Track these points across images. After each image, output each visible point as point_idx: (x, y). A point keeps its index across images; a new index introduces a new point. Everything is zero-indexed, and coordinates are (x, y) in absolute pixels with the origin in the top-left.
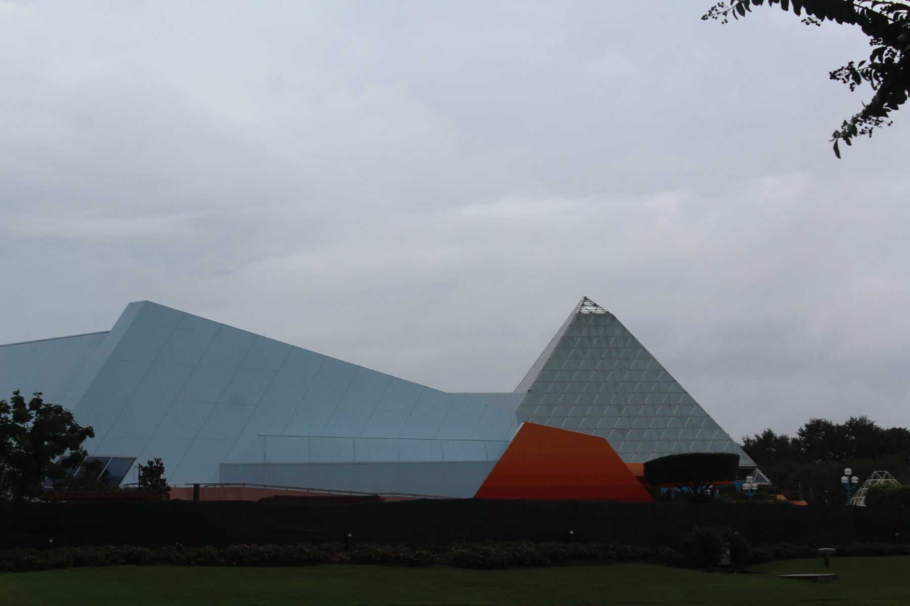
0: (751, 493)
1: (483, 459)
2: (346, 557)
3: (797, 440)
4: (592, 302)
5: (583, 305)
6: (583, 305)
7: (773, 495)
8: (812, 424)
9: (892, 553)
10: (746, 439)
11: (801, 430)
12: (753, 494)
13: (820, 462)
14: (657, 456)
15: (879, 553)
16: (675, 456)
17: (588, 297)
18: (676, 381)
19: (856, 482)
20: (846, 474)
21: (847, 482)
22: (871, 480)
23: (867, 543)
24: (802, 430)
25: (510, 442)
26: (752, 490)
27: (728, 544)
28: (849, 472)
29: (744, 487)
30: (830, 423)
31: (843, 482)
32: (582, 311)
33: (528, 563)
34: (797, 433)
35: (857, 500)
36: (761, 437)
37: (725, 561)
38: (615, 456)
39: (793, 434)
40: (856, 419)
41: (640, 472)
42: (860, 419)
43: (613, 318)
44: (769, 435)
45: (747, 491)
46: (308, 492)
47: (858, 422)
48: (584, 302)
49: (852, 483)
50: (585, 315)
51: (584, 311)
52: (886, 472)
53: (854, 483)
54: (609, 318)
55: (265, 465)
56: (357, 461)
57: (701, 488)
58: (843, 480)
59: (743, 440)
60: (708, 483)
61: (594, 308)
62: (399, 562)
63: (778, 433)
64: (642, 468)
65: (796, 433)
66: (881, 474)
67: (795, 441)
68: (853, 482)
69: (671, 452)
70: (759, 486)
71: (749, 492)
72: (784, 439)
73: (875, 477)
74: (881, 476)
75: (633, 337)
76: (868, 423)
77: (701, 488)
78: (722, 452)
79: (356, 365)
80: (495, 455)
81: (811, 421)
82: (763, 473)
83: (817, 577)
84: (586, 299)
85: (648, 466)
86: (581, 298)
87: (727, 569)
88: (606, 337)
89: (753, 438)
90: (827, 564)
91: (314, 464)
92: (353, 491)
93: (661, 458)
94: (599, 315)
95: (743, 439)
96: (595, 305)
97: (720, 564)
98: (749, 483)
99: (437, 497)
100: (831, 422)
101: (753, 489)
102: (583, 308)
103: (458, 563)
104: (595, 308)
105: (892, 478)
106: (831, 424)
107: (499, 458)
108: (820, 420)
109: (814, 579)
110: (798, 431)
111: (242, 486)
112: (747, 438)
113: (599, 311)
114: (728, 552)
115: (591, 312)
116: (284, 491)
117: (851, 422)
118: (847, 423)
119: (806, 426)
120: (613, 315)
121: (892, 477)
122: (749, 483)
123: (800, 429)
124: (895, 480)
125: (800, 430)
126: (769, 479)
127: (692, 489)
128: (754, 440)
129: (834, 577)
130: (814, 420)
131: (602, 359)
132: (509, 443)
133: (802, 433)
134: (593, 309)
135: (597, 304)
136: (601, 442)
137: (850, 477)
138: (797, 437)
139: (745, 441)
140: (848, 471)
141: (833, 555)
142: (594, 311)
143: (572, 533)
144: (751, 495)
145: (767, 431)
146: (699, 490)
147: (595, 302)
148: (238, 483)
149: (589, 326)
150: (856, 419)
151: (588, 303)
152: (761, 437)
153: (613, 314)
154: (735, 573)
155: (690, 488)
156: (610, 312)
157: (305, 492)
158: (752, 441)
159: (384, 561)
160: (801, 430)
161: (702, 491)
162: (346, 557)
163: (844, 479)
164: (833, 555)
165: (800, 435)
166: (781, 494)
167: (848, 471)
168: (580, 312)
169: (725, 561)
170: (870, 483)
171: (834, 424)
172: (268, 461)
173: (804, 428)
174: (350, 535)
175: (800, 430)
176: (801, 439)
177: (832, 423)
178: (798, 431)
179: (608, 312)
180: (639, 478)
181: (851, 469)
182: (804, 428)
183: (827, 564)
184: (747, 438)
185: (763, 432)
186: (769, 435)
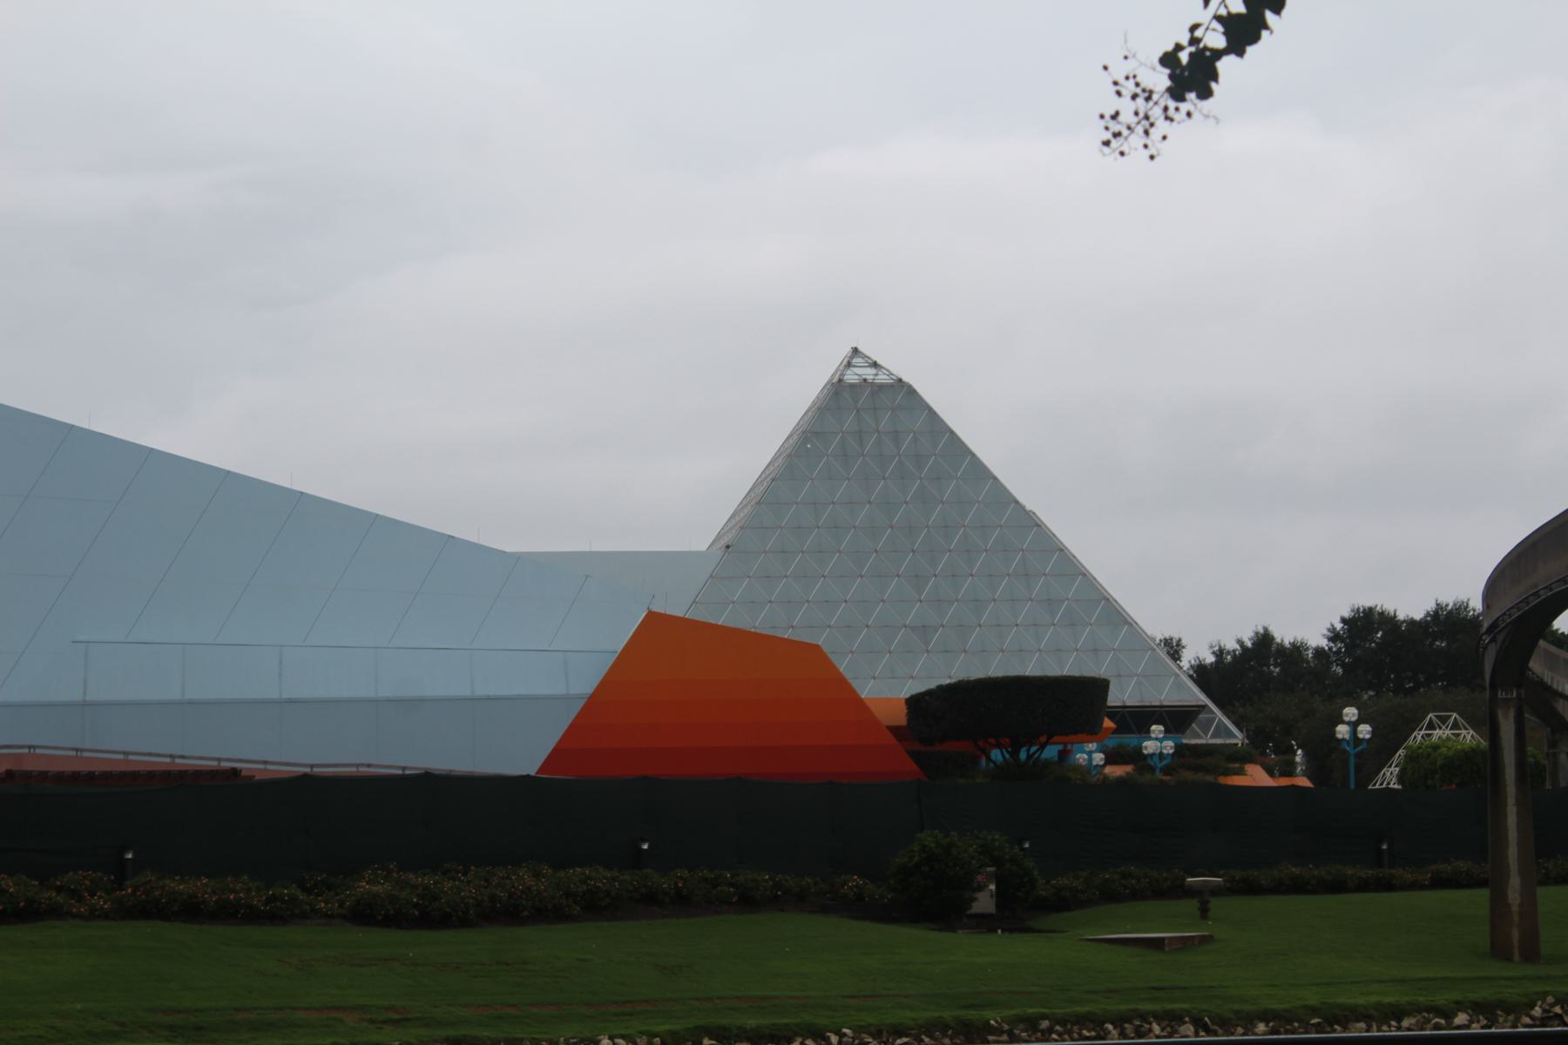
0: (1160, 763)
1: (560, 690)
2: (105, 903)
3: (1323, 649)
4: (868, 358)
5: (849, 365)
6: (849, 365)
7: (1237, 765)
8: (1354, 617)
9: (1364, 886)
10: (1217, 648)
11: (1332, 629)
12: (1164, 762)
13: (1370, 697)
14: (932, 684)
15: (1337, 887)
16: (1085, 677)
17: (861, 348)
18: (453, 537)
19: (1368, 736)
20: (1346, 719)
21: (1347, 737)
22: (1422, 732)
23: (1311, 866)
24: (1334, 629)
25: (619, 652)
26: (1161, 754)
27: (989, 869)
28: (1354, 715)
29: (1146, 748)
30: (1392, 614)
31: (1339, 736)
32: (846, 377)
33: (526, 913)
34: (1324, 635)
35: (1391, 773)
36: (1249, 644)
37: (984, 902)
38: (842, 683)
39: (1316, 638)
40: (1447, 605)
41: (900, 717)
42: (1455, 605)
43: (911, 392)
44: (1264, 640)
45: (1152, 755)
46: (128, 761)
47: (1451, 612)
48: (852, 357)
49: (1358, 738)
50: (852, 386)
51: (851, 377)
52: (1455, 715)
53: (1364, 739)
54: (902, 391)
55: (85, 704)
56: (286, 696)
57: (1028, 751)
58: (1340, 732)
59: (1212, 651)
60: (1043, 739)
61: (872, 371)
62: (227, 913)
63: (1284, 635)
64: (904, 710)
65: (1321, 637)
66: (1444, 720)
67: (1319, 652)
68: (1361, 736)
69: (950, 677)
70: (1180, 750)
71: (1156, 759)
72: (1297, 649)
73: (1431, 726)
74: (1444, 724)
75: (952, 432)
76: (1471, 613)
77: (1028, 751)
78: (1097, 676)
79: (296, 491)
80: (585, 682)
81: (1353, 611)
82: (1233, 723)
83: (1163, 939)
84: (855, 351)
85: (916, 704)
86: (847, 350)
87: (985, 924)
88: (896, 432)
89: (1231, 645)
90: (1204, 912)
91: (191, 703)
92: (374, 762)
93: (940, 688)
94: (882, 386)
95: (1211, 647)
96: (875, 365)
97: (969, 912)
98: (1157, 739)
99: (404, 768)
100: (1395, 612)
101: (1165, 752)
102: (849, 372)
103: (364, 915)
104: (873, 371)
105: (1466, 729)
106: (1395, 616)
107: (593, 690)
108: (1371, 609)
109: (1157, 944)
110: (1326, 632)
111: (26, 751)
112: (1220, 647)
113: (882, 378)
114: (992, 887)
115: (865, 380)
116: (120, 760)
117: (1436, 612)
118: (1428, 614)
119: (1344, 620)
120: (910, 386)
121: (1467, 725)
122: (1157, 739)
123: (1329, 626)
124: (1472, 732)
125: (1329, 630)
126: (1241, 731)
127: (1008, 752)
128: (1234, 651)
129: (1204, 940)
130: (1358, 609)
131: (884, 478)
132: (617, 655)
133: (1334, 637)
134: (869, 373)
135: (879, 362)
136: (812, 653)
137: (1354, 725)
138: (1324, 643)
139: (1214, 653)
140: (1351, 713)
141: (1216, 891)
142: (872, 377)
143: (645, 847)
144: (1160, 765)
145: (1262, 631)
146: (1023, 755)
147: (875, 359)
148: (99, 748)
149: (858, 411)
150: (1447, 605)
151: (860, 360)
152: (1249, 644)
153: (911, 383)
154: (999, 931)
155: (1004, 751)
156: (905, 379)
157: (167, 763)
158: (1228, 652)
159: (191, 911)
160: (1332, 629)
161: (1029, 757)
162: (105, 903)
163: (1342, 731)
164: (1216, 891)
165: (1330, 639)
166: (1256, 764)
167: (1351, 713)
168: (840, 381)
169: (984, 902)
170: (1419, 737)
171: (1401, 616)
172: (88, 698)
173: (1339, 626)
174: (130, 856)
175: (1329, 630)
176: (1330, 649)
177: (1397, 614)
178: (1326, 632)
179: (900, 380)
180: (895, 730)
181: (1358, 708)
182: (1339, 626)
183: (1204, 912)
184: (1220, 647)
185: (1252, 634)
186: (1264, 640)
